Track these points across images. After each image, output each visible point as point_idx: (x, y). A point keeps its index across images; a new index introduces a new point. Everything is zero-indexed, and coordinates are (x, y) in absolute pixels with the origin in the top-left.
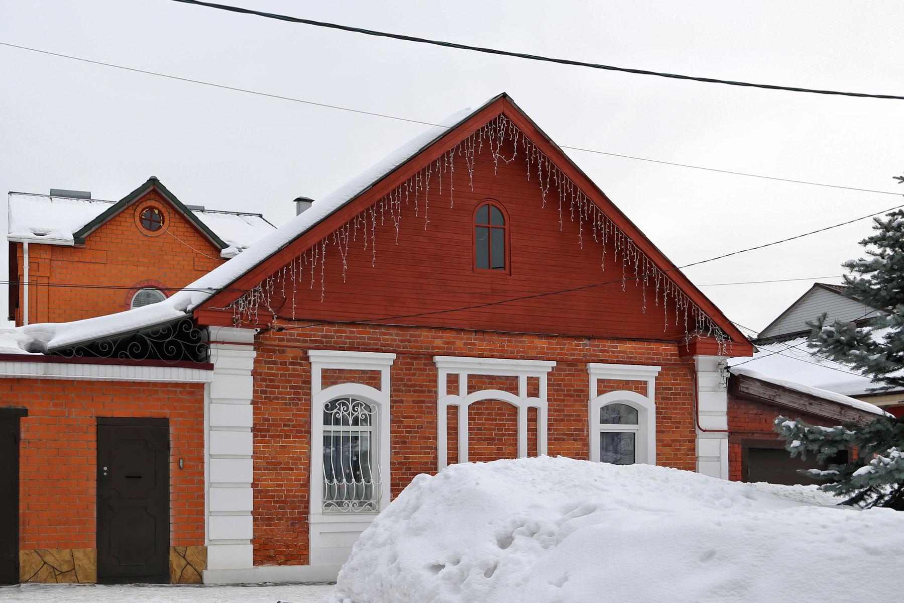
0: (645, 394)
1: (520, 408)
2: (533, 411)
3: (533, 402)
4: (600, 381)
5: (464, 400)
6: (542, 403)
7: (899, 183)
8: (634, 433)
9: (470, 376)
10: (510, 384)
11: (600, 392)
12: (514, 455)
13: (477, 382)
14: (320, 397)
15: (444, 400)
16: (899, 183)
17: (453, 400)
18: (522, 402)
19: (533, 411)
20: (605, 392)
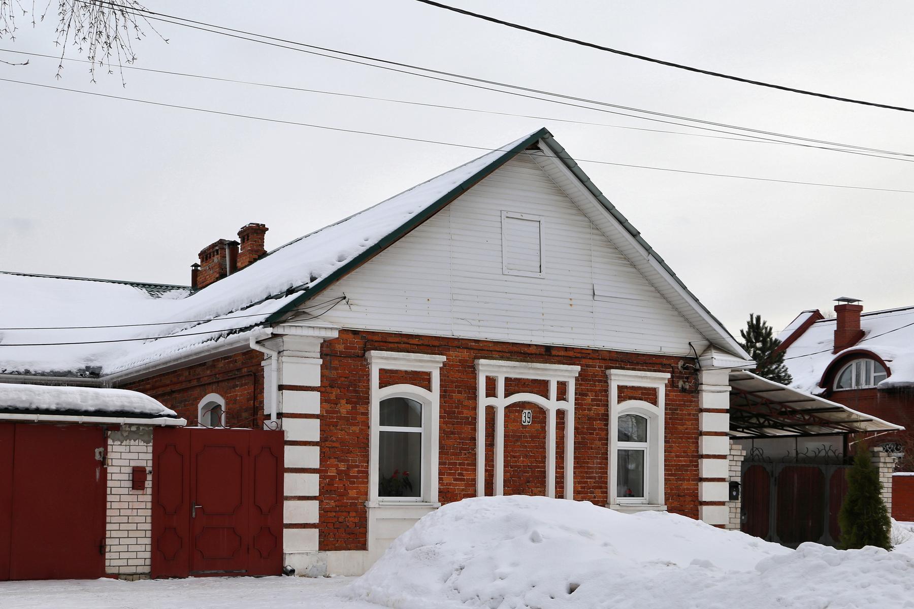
0: (429, 388)
1: (567, 411)
2: (561, 414)
3: (562, 405)
4: (620, 388)
5: (501, 402)
6: (569, 406)
7: (742, 331)
8: (643, 451)
9: (507, 380)
10: (541, 387)
11: (621, 399)
12: (543, 493)
13: (513, 386)
14: (378, 395)
15: (483, 401)
16: (742, 331)
17: (491, 401)
18: (551, 405)
19: (561, 414)
20: (383, 387)
